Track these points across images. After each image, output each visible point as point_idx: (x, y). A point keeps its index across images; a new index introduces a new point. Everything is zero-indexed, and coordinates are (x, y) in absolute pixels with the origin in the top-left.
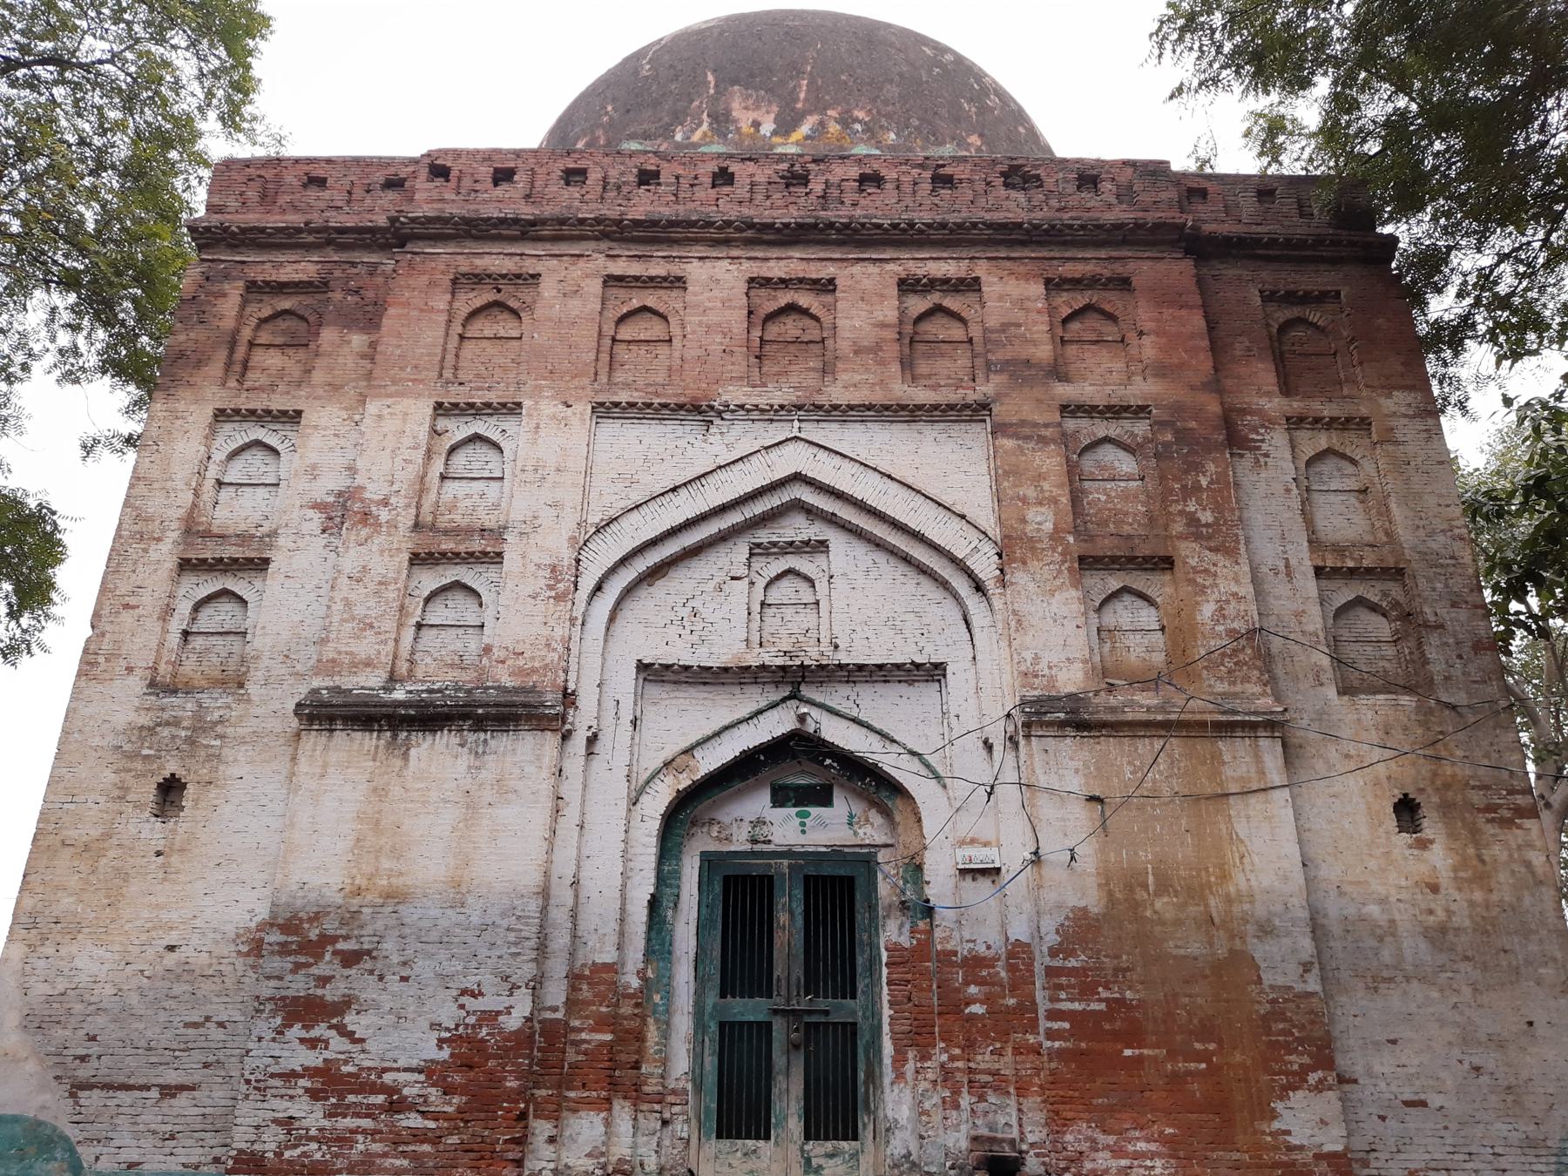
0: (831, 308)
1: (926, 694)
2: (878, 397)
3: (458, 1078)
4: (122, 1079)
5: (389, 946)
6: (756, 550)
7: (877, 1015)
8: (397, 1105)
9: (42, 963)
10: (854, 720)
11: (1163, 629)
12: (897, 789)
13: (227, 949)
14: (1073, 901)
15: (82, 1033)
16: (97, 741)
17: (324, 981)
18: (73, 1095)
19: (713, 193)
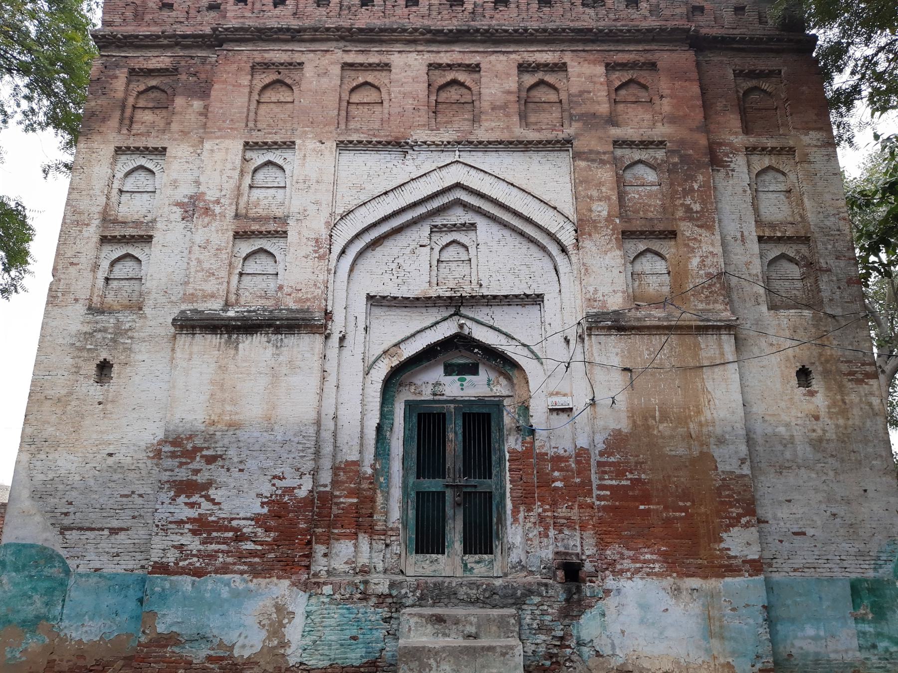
0: (478, 82)
2: (505, 136)
4: (88, 525)
5: (232, 453)
6: (435, 229)
8: (240, 537)
9: (39, 463)
10: (491, 327)
11: (669, 273)
12: (515, 365)
14: (613, 425)
15: (65, 500)
16: (61, 341)
17: (196, 472)
18: (62, 533)
19: (406, 10)
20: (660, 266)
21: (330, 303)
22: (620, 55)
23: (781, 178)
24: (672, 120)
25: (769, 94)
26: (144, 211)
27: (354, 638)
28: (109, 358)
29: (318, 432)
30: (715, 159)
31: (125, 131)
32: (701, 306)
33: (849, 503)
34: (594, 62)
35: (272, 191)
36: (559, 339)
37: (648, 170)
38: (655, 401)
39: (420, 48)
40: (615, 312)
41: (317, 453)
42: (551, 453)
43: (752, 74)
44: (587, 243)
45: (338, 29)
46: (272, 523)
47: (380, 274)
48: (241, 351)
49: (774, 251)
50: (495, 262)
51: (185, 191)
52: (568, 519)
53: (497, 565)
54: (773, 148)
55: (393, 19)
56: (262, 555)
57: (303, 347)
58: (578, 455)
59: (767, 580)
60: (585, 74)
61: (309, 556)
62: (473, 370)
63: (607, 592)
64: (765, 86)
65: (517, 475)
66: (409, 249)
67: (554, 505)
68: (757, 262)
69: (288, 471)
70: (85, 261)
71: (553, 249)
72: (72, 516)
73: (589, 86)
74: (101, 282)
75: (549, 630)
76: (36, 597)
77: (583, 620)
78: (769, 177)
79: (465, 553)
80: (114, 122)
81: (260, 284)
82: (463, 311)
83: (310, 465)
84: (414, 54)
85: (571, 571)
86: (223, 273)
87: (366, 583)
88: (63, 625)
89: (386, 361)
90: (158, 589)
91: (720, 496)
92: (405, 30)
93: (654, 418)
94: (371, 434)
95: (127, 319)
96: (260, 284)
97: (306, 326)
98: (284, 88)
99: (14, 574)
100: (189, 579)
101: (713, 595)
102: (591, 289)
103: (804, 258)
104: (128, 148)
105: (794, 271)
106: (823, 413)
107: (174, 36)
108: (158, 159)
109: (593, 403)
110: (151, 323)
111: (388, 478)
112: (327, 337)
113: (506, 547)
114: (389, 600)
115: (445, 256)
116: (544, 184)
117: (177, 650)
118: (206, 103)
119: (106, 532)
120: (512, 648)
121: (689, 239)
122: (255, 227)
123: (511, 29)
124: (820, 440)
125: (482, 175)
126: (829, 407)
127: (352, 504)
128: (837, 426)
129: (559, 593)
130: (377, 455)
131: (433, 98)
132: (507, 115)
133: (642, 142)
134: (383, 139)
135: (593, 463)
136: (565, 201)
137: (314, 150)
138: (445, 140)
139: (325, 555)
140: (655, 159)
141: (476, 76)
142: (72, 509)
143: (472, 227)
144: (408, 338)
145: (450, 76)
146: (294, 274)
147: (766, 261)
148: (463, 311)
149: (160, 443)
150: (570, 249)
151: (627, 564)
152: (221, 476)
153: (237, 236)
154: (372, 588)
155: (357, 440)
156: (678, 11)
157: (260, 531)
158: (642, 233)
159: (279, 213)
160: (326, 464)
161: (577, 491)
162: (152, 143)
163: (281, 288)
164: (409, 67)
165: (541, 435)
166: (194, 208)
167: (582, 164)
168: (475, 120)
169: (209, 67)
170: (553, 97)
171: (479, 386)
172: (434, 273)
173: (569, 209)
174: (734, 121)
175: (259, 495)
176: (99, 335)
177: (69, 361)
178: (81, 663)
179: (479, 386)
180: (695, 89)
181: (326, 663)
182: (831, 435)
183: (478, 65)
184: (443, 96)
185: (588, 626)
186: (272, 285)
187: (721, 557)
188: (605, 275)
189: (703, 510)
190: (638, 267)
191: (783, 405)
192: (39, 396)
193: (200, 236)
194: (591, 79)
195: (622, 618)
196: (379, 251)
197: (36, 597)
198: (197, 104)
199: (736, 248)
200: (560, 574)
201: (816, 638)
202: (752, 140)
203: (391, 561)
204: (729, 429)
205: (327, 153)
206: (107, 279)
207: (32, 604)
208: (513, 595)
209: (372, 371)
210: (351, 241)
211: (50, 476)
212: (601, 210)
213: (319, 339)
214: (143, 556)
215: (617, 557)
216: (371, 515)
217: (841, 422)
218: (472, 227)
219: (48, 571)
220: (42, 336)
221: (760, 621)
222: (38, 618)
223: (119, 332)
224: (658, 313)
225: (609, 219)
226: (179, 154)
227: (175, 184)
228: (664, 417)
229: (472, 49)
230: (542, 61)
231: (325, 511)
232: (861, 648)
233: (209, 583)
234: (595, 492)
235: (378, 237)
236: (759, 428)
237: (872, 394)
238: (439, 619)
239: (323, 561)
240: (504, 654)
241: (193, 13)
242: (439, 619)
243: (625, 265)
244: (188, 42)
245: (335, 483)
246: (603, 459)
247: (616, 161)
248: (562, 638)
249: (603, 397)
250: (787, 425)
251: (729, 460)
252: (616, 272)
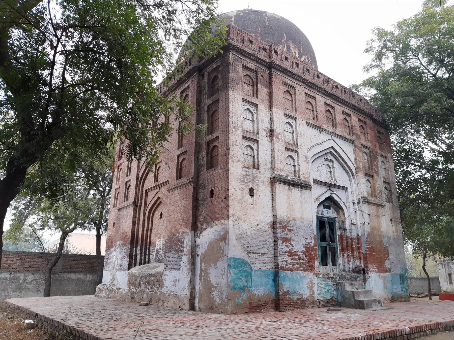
1: (344, 192)
2: (342, 135)
3: (307, 254)
4: (255, 251)
5: (295, 229)
7: (337, 246)
8: (300, 259)
9: (236, 226)
11: (371, 187)
12: (342, 209)
13: (267, 226)
16: (236, 177)
17: (287, 234)
18: (248, 254)
25: (381, 139)
28: (252, 187)
45: (304, 79)
60: (355, 120)
72: (250, 248)
76: (243, 279)
90: (282, 276)
99: (234, 270)
107: (257, 57)
110: (262, 176)
117: (289, 296)
119: (260, 255)
134: (317, 125)
175: (303, 244)
176: (248, 177)
197: (243, 279)
201: (396, 288)
207: (242, 282)
219: (246, 269)
222: (245, 287)
244: (260, 61)
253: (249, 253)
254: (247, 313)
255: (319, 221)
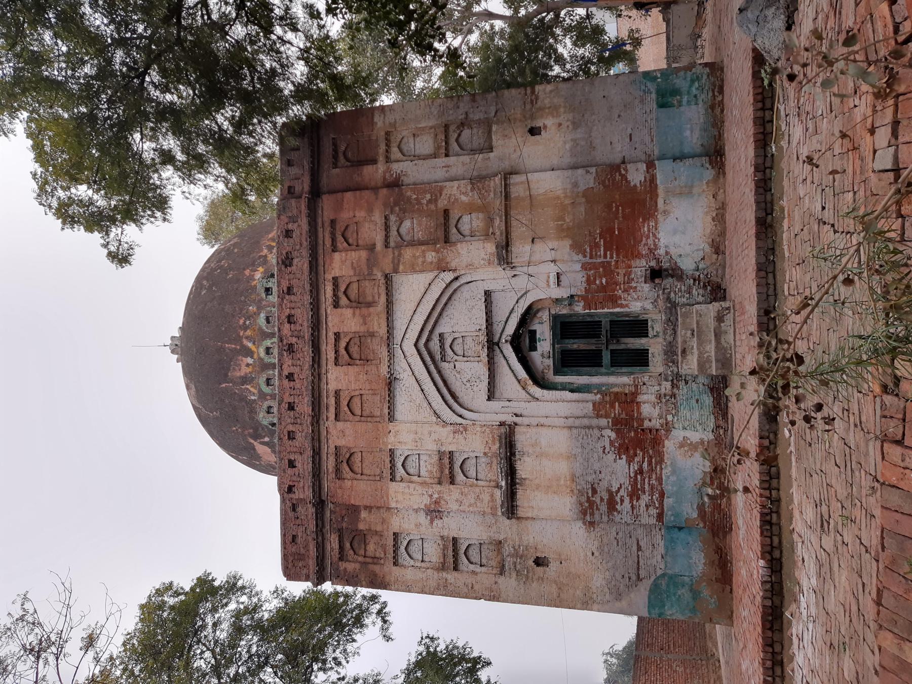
0: (346, 334)
2: (384, 316)
4: (636, 565)
5: (590, 479)
6: (443, 359)
7: (607, 314)
8: (640, 471)
10: (506, 323)
12: (530, 308)
14: (568, 249)
16: (522, 591)
17: (602, 500)
20: (466, 219)
21: (494, 423)
22: (326, 243)
23: (405, 140)
24: (370, 211)
26: (435, 546)
27: (697, 401)
29: (576, 427)
30: (395, 184)
31: (382, 561)
32: (492, 195)
33: (611, 107)
34: (332, 259)
35: (422, 463)
36: (513, 281)
37: (403, 225)
38: (552, 224)
39: (323, 371)
40: (497, 247)
41: (589, 427)
42: (585, 285)
43: (335, 157)
44: (453, 265)
45: (312, 425)
46: (632, 452)
47: (474, 392)
48: (527, 476)
49: (454, 146)
50: (464, 320)
51: (423, 519)
52: (625, 275)
53: (654, 317)
54: (387, 145)
55: (303, 389)
56: (651, 457)
57: (522, 439)
58: (586, 269)
59: (658, 159)
60: (340, 265)
61: (651, 431)
62: (533, 333)
63: (667, 253)
64: (343, 148)
65: (599, 305)
66: (458, 376)
67: (616, 284)
68: (462, 158)
69: (599, 445)
70: (470, 580)
71: (456, 285)
73: (348, 263)
74: (483, 569)
75: (690, 287)
77: (683, 267)
78: (405, 148)
79: (647, 336)
80: (376, 568)
81: (482, 468)
82: (496, 340)
83: (596, 431)
84: (329, 375)
85: (655, 274)
86: (477, 490)
87: (665, 395)
88: (695, 575)
89: (529, 388)
90: (672, 519)
91: (609, 186)
92: (313, 381)
93: (562, 225)
94: (576, 396)
95: (507, 550)
96: (482, 468)
97: (510, 437)
98: (352, 458)
100: (665, 500)
101: (667, 191)
102: (482, 262)
103: (458, 128)
104: (394, 557)
105: (466, 133)
106: (557, 121)
108: (400, 538)
109: (554, 261)
111: (603, 385)
112: (516, 424)
113: (643, 312)
114: (675, 381)
115: (460, 352)
116: (414, 291)
118: (362, 508)
119: (640, 553)
120: (697, 311)
121: (449, 202)
122: (447, 471)
123: (311, 313)
124: (574, 123)
125: (409, 330)
126: (553, 117)
127: (619, 406)
128: (565, 112)
129: (668, 282)
130: (589, 392)
131: (358, 362)
132: (370, 315)
133: (386, 230)
135: (591, 261)
136: (423, 279)
137: (395, 437)
138: (387, 354)
139: (650, 420)
140: (396, 221)
141: (342, 335)
142: (627, 576)
143: (441, 335)
144: (515, 375)
145: (342, 351)
146: (476, 446)
147: (461, 152)
148: (496, 340)
149: (584, 523)
150: (456, 275)
151: (650, 242)
152: (604, 484)
153: (452, 482)
154: (669, 392)
155: (580, 404)
156: (294, 204)
157: (636, 459)
158: (445, 230)
159: (435, 458)
160: (595, 422)
161: (608, 271)
162: (390, 542)
163: (485, 454)
164: (337, 378)
165: (574, 291)
166: (434, 512)
167: (401, 268)
168: (372, 335)
169: (338, 509)
170: (355, 286)
171: (543, 329)
172: (472, 359)
173: (430, 276)
174: (368, 170)
175: (615, 461)
176: (518, 567)
177: (535, 585)
178: (717, 562)
179: (543, 329)
180: (349, 195)
181: (712, 416)
182: (570, 116)
183: (335, 334)
184: (356, 356)
185: (687, 265)
186: (483, 460)
187: (645, 186)
188: (473, 254)
189: (617, 196)
190: (467, 232)
191: (552, 145)
192: (557, 601)
193: (454, 506)
194: (343, 262)
195: (682, 245)
196: (459, 394)
197: (679, 592)
198: (364, 514)
199: (453, 172)
200: (657, 281)
202: (381, 159)
203: (654, 382)
204: (568, 180)
205: (396, 429)
206: (481, 566)
208: (670, 309)
209: (536, 396)
210: (454, 411)
211: (607, 590)
212: (431, 256)
213: (517, 429)
214: (653, 529)
215: (646, 247)
216: (626, 394)
217: (562, 110)
218: (441, 335)
219: (664, 587)
220: (519, 603)
221: (682, 164)
223: (516, 554)
224: (497, 222)
225: (437, 251)
226: (398, 524)
227: (418, 525)
228: (562, 218)
229: (324, 337)
230: (332, 293)
231: (624, 422)
232: (696, 104)
233: (668, 488)
234: (608, 259)
235: (450, 395)
236: (567, 160)
237: (544, 90)
238: (684, 351)
239: (654, 421)
240: (701, 315)
241: (299, 522)
242: (684, 351)
243: (466, 241)
244: (320, 523)
245: (606, 416)
246: (588, 255)
247: (398, 247)
248: (695, 280)
249: (550, 255)
250: (565, 143)
251: (586, 180)
252: (471, 247)
253: (639, 579)
254: (731, 589)
255: (563, 366)
